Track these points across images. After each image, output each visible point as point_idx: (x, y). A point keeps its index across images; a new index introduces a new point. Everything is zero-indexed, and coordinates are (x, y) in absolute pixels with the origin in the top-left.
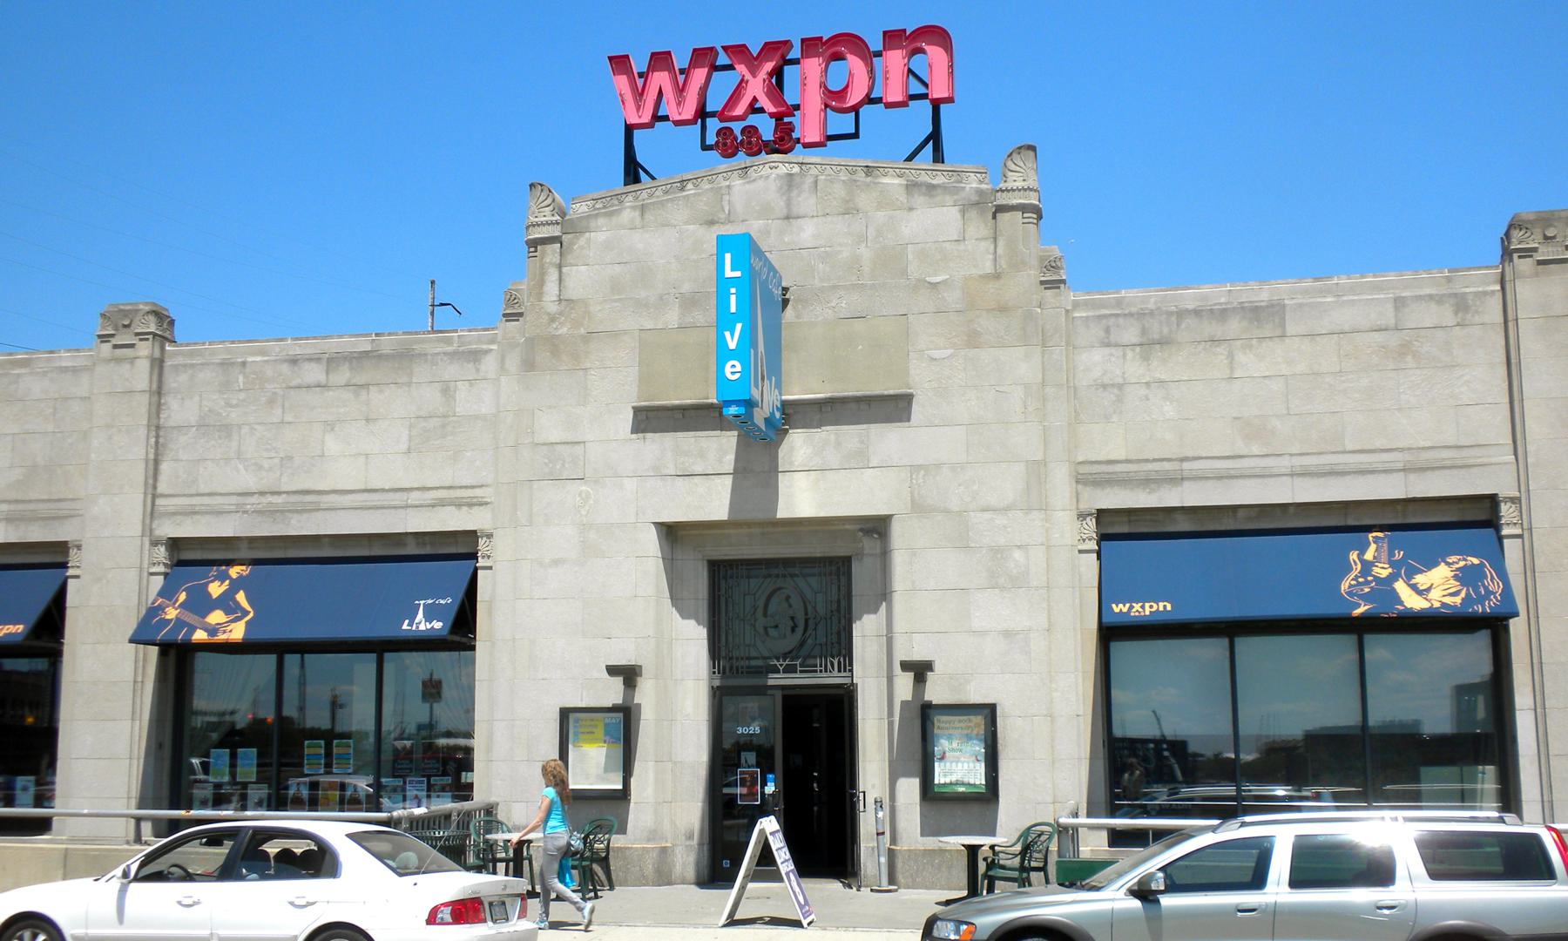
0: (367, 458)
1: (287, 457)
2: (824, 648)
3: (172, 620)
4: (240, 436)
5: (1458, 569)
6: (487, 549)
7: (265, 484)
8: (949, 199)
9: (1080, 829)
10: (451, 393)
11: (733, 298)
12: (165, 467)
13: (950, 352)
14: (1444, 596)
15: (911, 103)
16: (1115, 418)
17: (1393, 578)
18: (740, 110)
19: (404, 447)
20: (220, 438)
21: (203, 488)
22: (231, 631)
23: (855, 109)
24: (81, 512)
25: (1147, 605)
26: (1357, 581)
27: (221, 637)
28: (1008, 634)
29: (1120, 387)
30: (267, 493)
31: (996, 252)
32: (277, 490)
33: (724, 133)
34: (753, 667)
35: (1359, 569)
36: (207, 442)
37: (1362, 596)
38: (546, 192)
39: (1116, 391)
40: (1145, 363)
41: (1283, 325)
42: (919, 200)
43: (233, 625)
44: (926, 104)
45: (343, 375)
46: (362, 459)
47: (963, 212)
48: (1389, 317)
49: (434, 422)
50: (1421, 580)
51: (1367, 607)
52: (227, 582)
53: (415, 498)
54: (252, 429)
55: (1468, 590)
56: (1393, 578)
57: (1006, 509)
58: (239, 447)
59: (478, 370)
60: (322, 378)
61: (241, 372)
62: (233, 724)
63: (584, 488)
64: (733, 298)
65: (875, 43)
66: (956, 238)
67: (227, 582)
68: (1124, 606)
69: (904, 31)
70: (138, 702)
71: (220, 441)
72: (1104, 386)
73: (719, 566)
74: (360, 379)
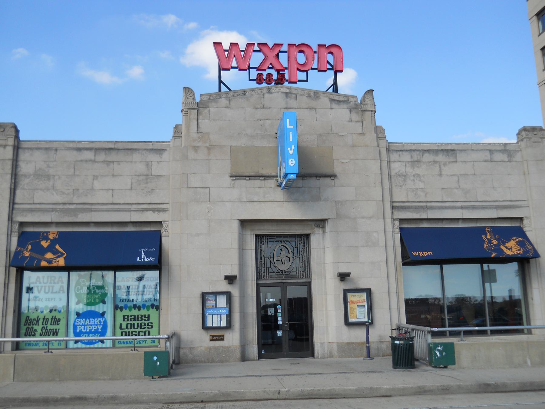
0: (113, 191)
2: (297, 268)
3: (28, 257)
5: (517, 242)
6: (165, 227)
7: (65, 200)
8: (345, 106)
9: (532, 329)
10: (150, 166)
11: (291, 135)
12: (18, 192)
13: (348, 160)
14: (516, 250)
15: (231, 69)
16: (403, 187)
17: (499, 245)
18: (265, 67)
19: (129, 187)
20: (44, 180)
21: (36, 201)
22: (58, 261)
23: (307, 71)
24: (169, 209)
26: (488, 245)
27: (54, 264)
29: (405, 176)
30: (66, 204)
31: (363, 126)
32: (72, 202)
33: (260, 75)
34: (293, 275)
35: (487, 241)
37: (492, 250)
38: (190, 91)
39: (403, 177)
40: (413, 168)
41: (456, 157)
42: (334, 105)
43: (58, 259)
44: (332, 72)
45: (102, 157)
46: (111, 191)
47: (351, 111)
48: (488, 158)
49: (141, 178)
50: (507, 245)
51: (495, 254)
52: (49, 241)
53: (134, 207)
55: (523, 249)
56: (499, 245)
57: (371, 218)
58: (54, 185)
59: (161, 158)
61: (54, 154)
64: (291, 135)
65: (315, 49)
66: (348, 120)
67: (49, 241)
68: (416, 253)
69: (325, 45)
70: (6, 290)
71: (45, 182)
72: (399, 175)
73: (258, 237)
74: (109, 159)
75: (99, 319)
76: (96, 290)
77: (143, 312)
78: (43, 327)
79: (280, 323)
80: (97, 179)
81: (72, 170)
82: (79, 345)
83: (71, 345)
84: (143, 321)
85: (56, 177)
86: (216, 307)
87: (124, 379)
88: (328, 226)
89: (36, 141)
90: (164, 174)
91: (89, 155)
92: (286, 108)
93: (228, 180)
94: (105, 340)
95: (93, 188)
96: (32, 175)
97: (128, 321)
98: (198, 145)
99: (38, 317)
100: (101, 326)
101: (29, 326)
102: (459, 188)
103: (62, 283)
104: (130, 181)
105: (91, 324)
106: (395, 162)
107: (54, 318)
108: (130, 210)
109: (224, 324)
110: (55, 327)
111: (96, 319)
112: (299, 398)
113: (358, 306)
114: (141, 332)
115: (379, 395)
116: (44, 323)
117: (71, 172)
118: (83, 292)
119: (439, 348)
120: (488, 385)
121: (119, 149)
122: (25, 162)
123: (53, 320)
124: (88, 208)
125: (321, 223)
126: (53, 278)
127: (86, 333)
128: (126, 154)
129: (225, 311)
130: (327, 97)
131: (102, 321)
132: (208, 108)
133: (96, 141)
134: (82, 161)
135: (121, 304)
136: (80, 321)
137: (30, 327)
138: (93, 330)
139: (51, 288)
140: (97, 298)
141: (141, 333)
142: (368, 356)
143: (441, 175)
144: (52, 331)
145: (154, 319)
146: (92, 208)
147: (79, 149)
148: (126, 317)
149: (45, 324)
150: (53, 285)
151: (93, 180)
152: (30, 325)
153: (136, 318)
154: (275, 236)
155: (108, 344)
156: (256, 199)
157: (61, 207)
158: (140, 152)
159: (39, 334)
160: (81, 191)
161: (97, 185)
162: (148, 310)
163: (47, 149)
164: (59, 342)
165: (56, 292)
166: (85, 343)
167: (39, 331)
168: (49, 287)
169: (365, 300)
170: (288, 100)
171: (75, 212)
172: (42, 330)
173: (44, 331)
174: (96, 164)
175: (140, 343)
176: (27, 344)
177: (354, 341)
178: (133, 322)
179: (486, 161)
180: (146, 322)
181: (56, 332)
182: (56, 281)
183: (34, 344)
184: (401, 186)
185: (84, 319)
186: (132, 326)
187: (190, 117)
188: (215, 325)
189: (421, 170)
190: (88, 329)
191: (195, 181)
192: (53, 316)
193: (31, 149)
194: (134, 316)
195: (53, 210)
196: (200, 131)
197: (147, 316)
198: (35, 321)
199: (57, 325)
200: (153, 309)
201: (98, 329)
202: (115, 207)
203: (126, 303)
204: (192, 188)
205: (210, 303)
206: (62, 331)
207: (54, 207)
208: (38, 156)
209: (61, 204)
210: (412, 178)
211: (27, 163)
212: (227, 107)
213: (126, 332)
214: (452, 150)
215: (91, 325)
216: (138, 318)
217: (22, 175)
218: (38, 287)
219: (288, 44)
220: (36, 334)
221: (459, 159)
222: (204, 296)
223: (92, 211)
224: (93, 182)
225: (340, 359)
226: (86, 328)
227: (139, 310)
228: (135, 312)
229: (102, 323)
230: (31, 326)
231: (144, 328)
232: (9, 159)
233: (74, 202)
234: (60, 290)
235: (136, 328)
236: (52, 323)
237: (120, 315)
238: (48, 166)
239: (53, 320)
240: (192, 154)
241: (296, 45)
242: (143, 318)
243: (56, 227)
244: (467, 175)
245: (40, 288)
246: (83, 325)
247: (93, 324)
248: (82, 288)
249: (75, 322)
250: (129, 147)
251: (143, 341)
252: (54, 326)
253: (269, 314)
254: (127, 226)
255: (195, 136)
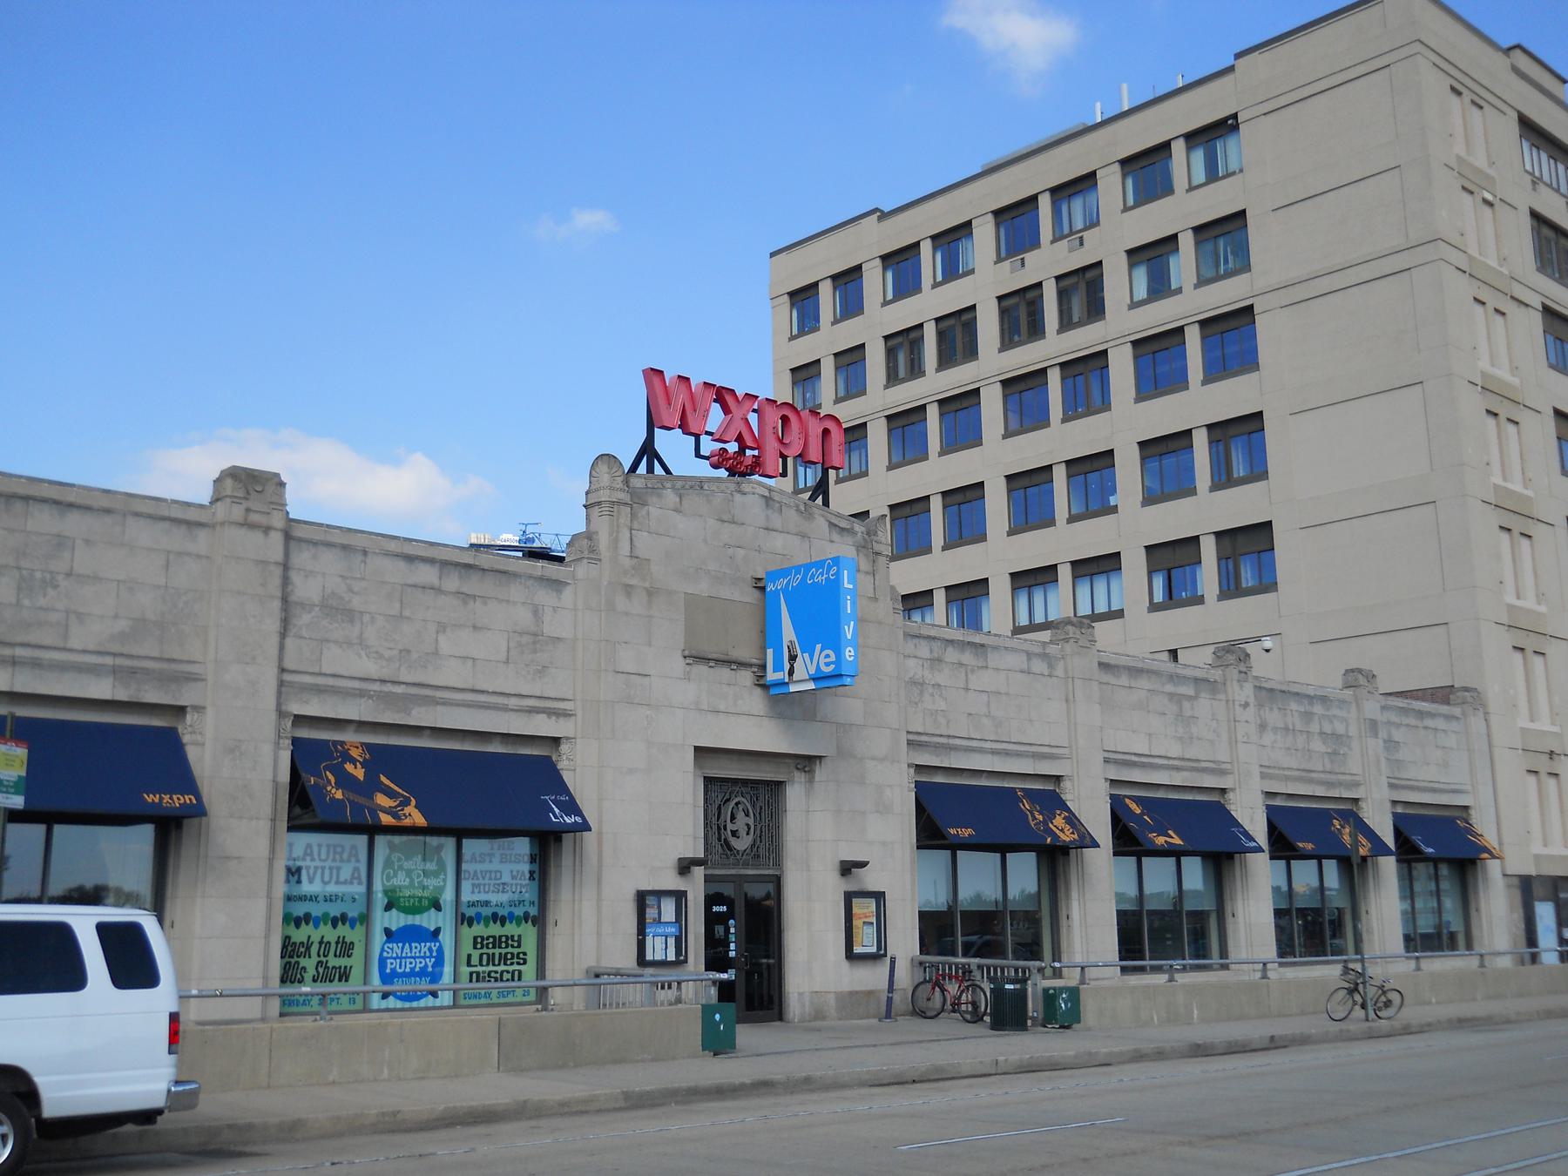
1: (404, 650)
4: (362, 623)
7: (385, 673)
19: (503, 657)
20: (343, 621)
25: (175, 797)
28: (884, 844)
32: (396, 680)
36: (331, 624)
41: (986, 660)
45: (452, 582)
46: (470, 663)
47: (858, 551)
53: (513, 702)
54: (372, 618)
60: (436, 582)
61: (362, 561)
62: (1030, 895)
63: (648, 712)
71: (343, 625)
74: (465, 589)
75: (428, 944)
76: (423, 880)
77: (510, 929)
78: (319, 962)
79: (732, 954)
80: (444, 631)
81: (397, 605)
82: (392, 1002)
83: (376, 1002)
84: (510, 950)
85: (366, 618)
86: (660, 922)
87: (674, 1058)
88: (820, 773)
89: (321, 525)
90: (564, 635)
91: (428, 574)
92: (767, 529)
93: (679, 663)
94: (439, 992)
95: (436, 653)
96: (317, 606)
97: (482, 948)
98: (632, 582)
99: (309, 937)
100: (433, 960)
101: (291, 960)
102: (988, 715)
103: (358, 861)
104: (505, 644)
105: (413, 955)
106: (909, 656)
107: (341, 940)
108: (505, 709)
109: (671, 957)
110: (343, 962)
111: (423, 944)
112: (1018, 1070)
113: (864, 923)
114: (505, 973)
115: (1098, 1063)
116: (321, 953)
117: (395, 610)
118: (399, 883)
119: (1064, 996)
120: (1198, 1046)
121: (483, 570)
122: (302, 572)
123: (340, 946)
124: (427, 696)
125: (806, 763)
126: (339, 850)
127: (405, 975)
128: (498, 583)
129: (673, 930)
130: (823, 516)
131: (434, 949)
132: (646, 508)
133: (439, 544)
134: (415, 586)
135: (470, 912)
136: (392, 949)
137: (293, 961)
138: (417, 969)
139: (335, 871)
140: (426, 898)
141: (506, 976)
142: (888, 1015)
143: (967, 689)
144: (338, 970)
145: (529, 945)
146: (434, 697)
147: (410, 559)
148: (479, 940)
149: (325, 956)
150: (338, 864)
151: (437, 632)
152: (293, 957)
153: (497, 942)
154: (728, 782)
155: (445, 998)
156: (722, 708)
157: (376, 687)
158: (523, 581)
159: (311, 978)
160: (415, 656)
161: (445, 645)
162: (519, 924)
163: (345, 547)
164: (352, 996)
165: (345, 882)
166: (401, 998)
167: (311, 972)
168: (331, 868)
169: (873, 912)
170: (770, 512)
171: (407, 701)
172: (317, 968)
173: (321, 970)
174: (443, 596)
175: (504, 996)
176: (287, 1002)
177: (858, 989)
178: (491, 951)
179: (1022, 672)
180: (515, 951)
181: (345, 972)
182: (345, 856)
183: (301, 1002)
184: (916, 704)
185: (400, 945)
186: (491, 960)
187: (618, 520)
188: (658, 958)
189: (943, 677)
190: (408, 966)
191: (627, 661)
192: (339, 937)
193: (315, 543)
194: (494, 937)
195: (362, 694)
196: (636, 553)
197: (516, 938)
198: (303, 947)
199: (349, 956)
200: (526, 922)
201: (426, 965)
202: (477, 698)
203: (480, 909)
204: (623, 673)
205: (651, 913)
206: (357, 974)
207: (364, 685)
208: (329, 562)
209: (376, 680)
210: (931, 690)
211: (306, 576)
212: (676, 510)
213: (478, 974)
214: (983, 646)
215: (414, 958)
216: (500, 942)
217: (296, 603)
218: (308, 868)
219: (1009, 478)
220: (306, 979)
221: (991, 664)
222: (642, 898)
223: (438, 703)
224: (437, 637)
225: (841, 1022)
226: (403, 963)
227: (503, 925)
228: (495, 930)
229: (434, 954)
230: (296, 959)
231: (512, 964)
232: (276, 563)
233: (402, 679)
234: (353, 877)
235: (497, 963)
236: (338, 953)
237: (468, 933)
238: (350, 590)
239: (340, 946)
240: (621, 602)
241: (778, 403)
242: (510, 942)
243: (502, 743)
244: (999, 693)
245: (311, 871)
246: (397, 957)
247: (417, 955)
248: (395, 875)
249: (383, 950)
250: (502, 567)
251: (508, 993)
252: (341, 959)
253: (717, 936)
254: (491, 742)
255: (627, 562)
